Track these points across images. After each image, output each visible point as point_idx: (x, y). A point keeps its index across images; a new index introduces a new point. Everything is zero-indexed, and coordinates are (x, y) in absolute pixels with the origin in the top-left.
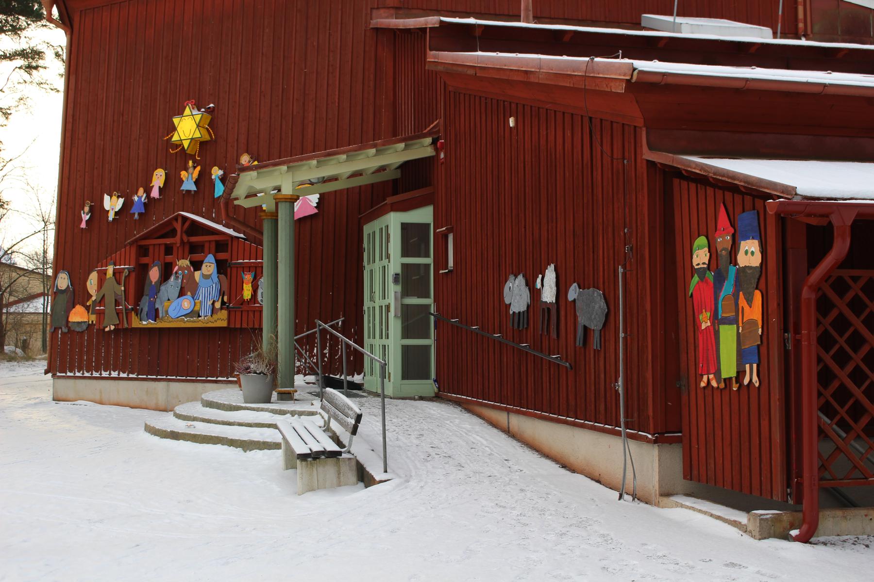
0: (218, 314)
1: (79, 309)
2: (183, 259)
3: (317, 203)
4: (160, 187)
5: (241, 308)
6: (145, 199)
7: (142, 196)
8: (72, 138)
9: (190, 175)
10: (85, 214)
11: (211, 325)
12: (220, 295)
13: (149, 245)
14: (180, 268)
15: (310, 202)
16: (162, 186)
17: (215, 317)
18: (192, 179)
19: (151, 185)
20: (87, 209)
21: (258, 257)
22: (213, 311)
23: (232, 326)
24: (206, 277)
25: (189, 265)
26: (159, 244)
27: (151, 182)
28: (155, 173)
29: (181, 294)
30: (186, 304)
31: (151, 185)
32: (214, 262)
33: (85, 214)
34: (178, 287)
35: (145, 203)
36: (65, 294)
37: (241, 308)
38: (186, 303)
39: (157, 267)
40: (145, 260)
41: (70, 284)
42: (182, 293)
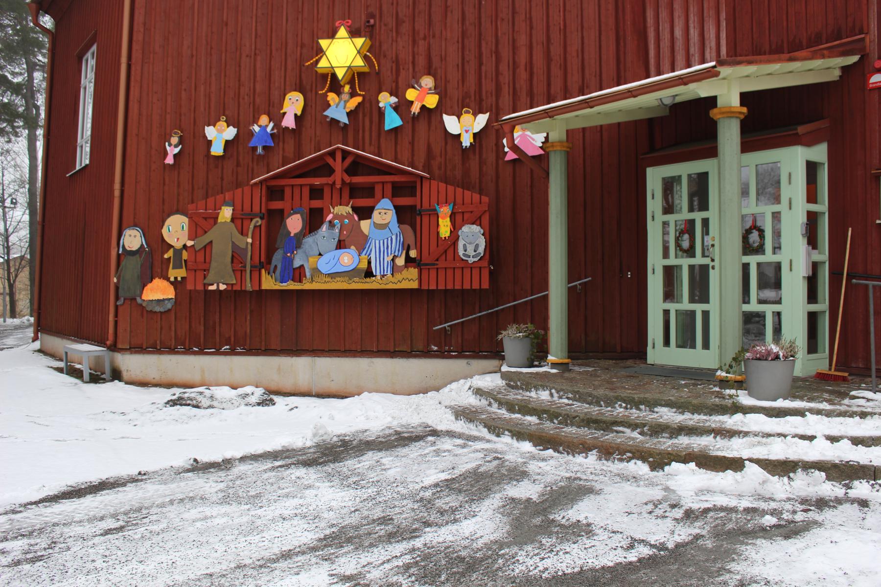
0: (403, 273)
1: (158, 282)
2: (340, 205)
3: (542, 142)
4: (296, 115)
5: (437, 265)
6: (273, 129)
7: (267, 126)
8: (143, 52)
9: (342, 102)
10: (173, 147)
11: (391, 286)
12: (403, 249)
13: (284, 186)
14: (336, 217)
15: (531, 141)
16: (299, 114)
17: (398, 276)
18: (344, 108)
19: (282, 112)
20: (175, 140)
21: (581, 134)
22: (394, 269)
23: (425, 287)
24: (383, 227)
25: (351, 212)
26: (301, 186)
27: (282, 108)
28: (288, 97)
29: (339, 246)
30: (348, 259)
31: (282, 112)
32: (392, 208)
33: (173, 147)
34: (334, 239)
35: (272, 135)
36: (138, 256)
37: (437, 265)
38: (346, 261)
39: (298, 216)
40: (276, 205)
41: (144, 243)
42: (341, 245)
